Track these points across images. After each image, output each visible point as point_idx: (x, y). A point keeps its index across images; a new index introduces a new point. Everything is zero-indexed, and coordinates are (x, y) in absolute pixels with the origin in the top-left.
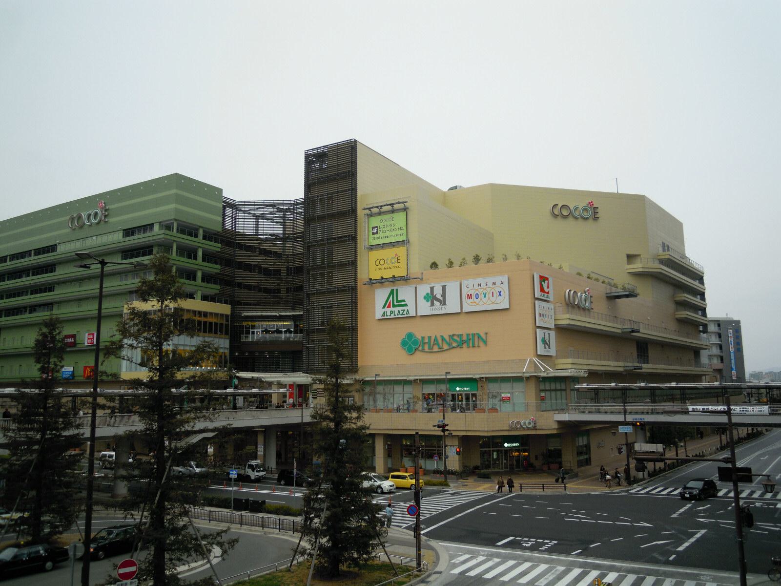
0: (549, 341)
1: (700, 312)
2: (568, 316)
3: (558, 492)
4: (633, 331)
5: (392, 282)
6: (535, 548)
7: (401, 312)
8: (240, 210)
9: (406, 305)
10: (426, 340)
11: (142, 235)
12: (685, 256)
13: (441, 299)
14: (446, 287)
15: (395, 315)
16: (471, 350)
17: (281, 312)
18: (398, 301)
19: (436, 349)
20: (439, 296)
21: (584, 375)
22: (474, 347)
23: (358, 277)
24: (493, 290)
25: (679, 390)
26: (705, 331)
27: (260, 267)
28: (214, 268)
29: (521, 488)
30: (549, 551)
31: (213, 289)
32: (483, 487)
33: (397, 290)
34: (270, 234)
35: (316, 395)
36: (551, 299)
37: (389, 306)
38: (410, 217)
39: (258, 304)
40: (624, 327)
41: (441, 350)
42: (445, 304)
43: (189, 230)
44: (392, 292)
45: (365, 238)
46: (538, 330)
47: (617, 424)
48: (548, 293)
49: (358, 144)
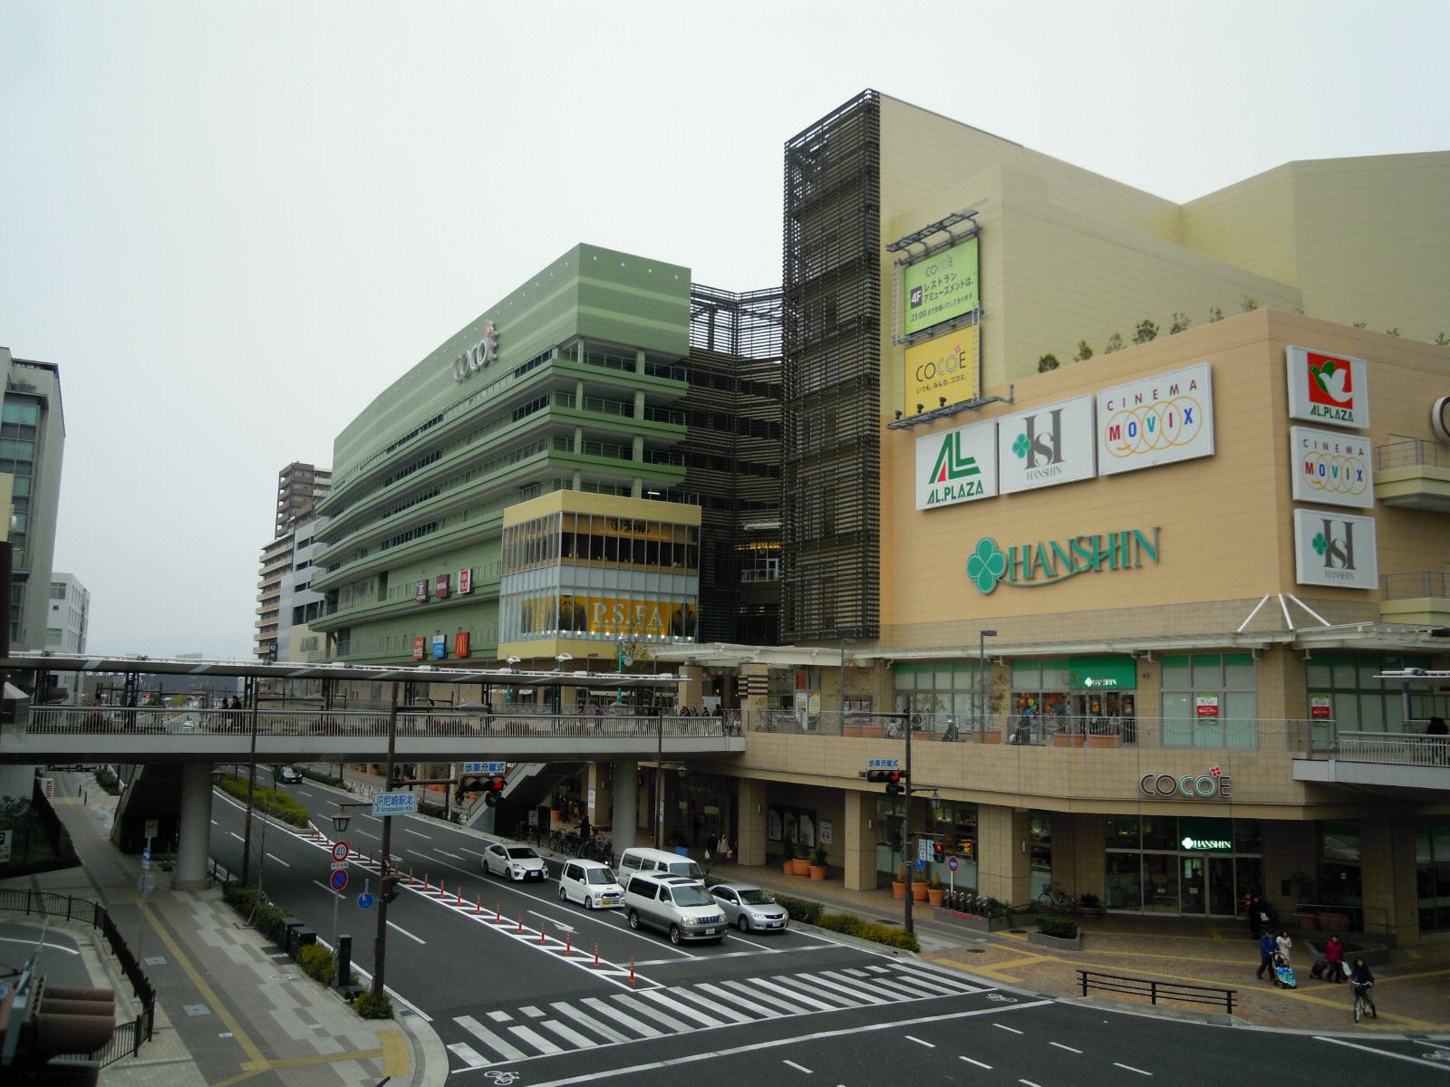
2: (1418, 470)
3: (1199, 1015)
7: (966, 489)
8: (745, 312)
9: (976, 470)
13: (1050, 445)
14: (1062, 413)
15: (953, 498)
16: (1122, 575)
18: (960, 463)
19: (1041, 578)
20: (1046, 441)
22: (1128, 568)
23: (881, 413)
24: (1171, 409)
28: (672, 432)
29: (1085, 987)
31: (673, 474)
33: (958, 434)
35: (746, 685)
36: (1361, 417)
37: (942, 478)
38: (986, 252)
41: (1053, 579)
42: (1058, 459)
45: (897, 319)
46: (1298, 512)
48: (1349, 404)
49: (882, 99)
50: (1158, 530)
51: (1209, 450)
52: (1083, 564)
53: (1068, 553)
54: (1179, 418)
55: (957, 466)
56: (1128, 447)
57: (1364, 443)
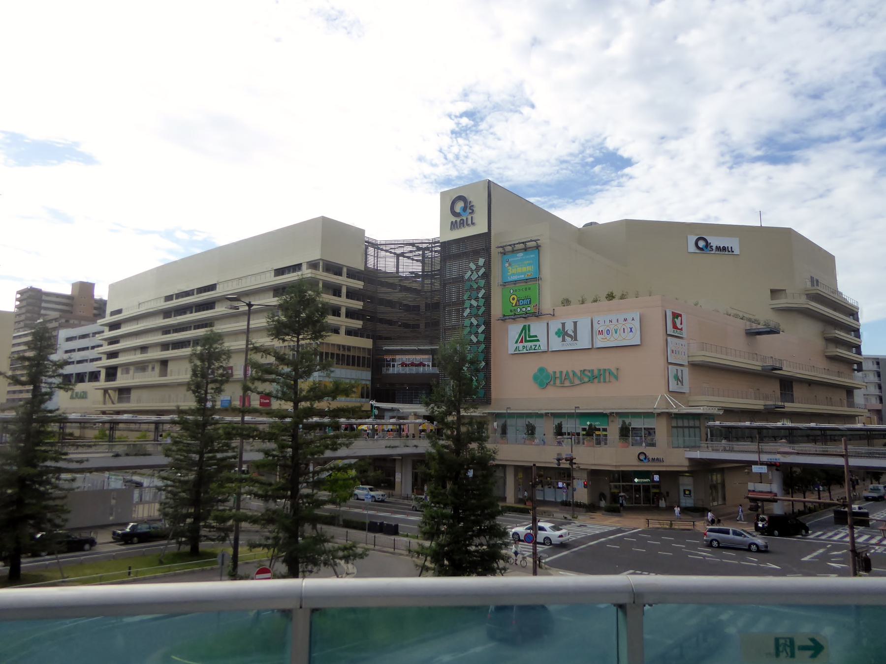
0: (682, 378)
1: (854, 349)
5: (524, 318)
7: (533, 347)
8: (382, 250)
9: (538, 340)
10: (558, 375)
12: (838, 291)
13: (573, 334)
17: (420, 346)
18: (530, 337)
21: (719, 412)
22: (605, 382)
24: (624, 327)
26: (860, 369)
27: (401, 304)
32: (610, 521)
33: (529, 326)
34: (410, 272)
36: (684, 336)
37: (522, 342)
39: (401, 339)
41: (572, 384)
42: (576, 339)
43: (333, 268)
44: (524, 328)
47: (750, 463)
48: (681, 329)
50: (618, 369)
51: (639, 343)
53: (580, 375)
54: (627, 330)
55: (529, 338)
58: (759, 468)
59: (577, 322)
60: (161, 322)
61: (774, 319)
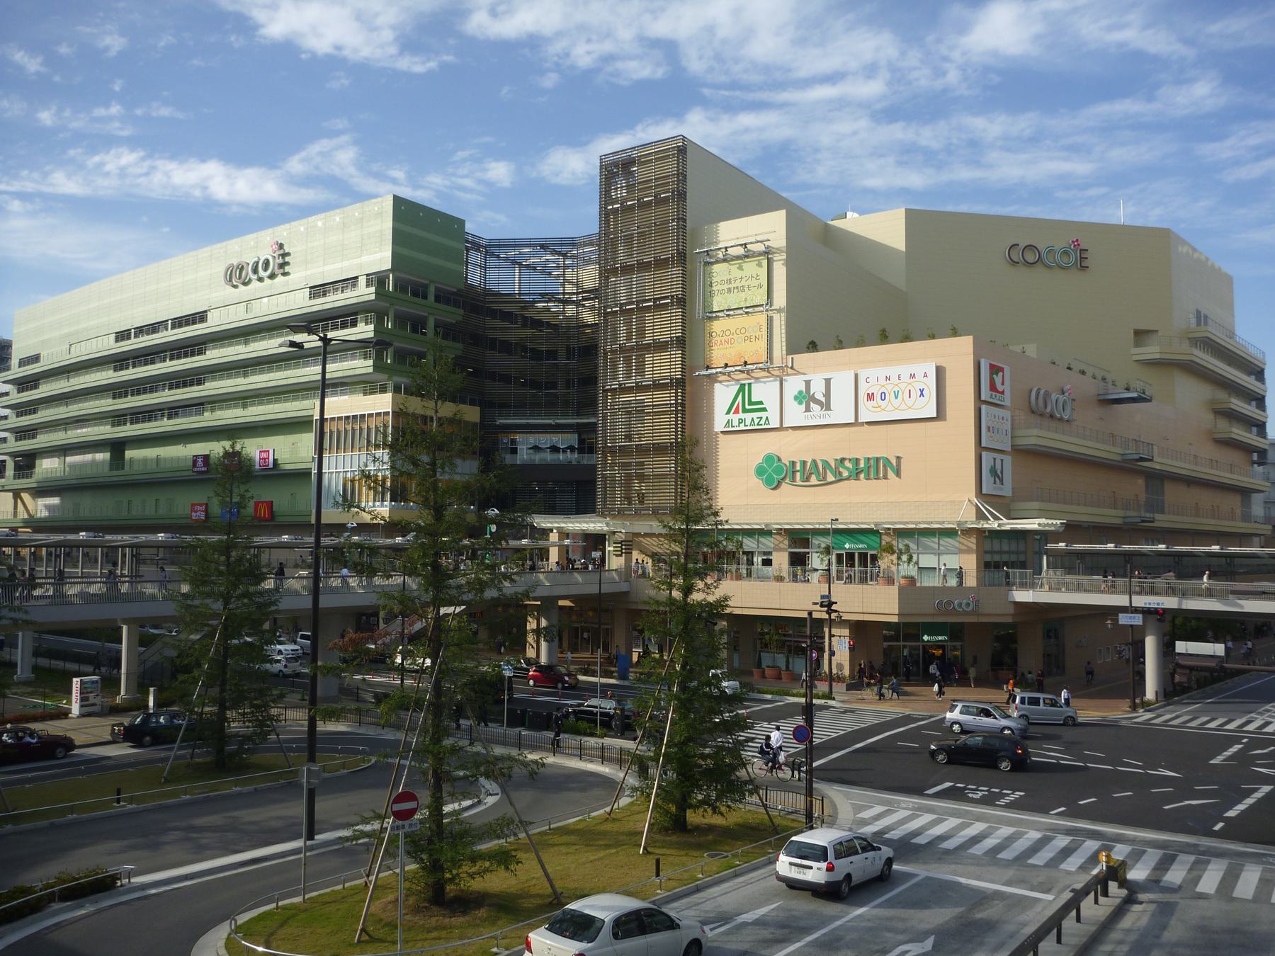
0: (1002, 473)
2: (1035, 432)
4: (1142, 459)
6: (988, 801)
9: (764, 410)
11: (339, 296)
13: (823, 400)
15: (745, 426)
18: (751, 403)
19: (814, 480)
20: (820, 396)
22: (877, 478)
24: (910, 387)
25: (1224, 559)
30: (1011, 806)
36: (1007, 402)
37: (737, 412)
40: (1127, 452)
42: (828, 408)
46: (984, 454)
48: (1003, 393)
52: (846, 474)
54: (917, 393)
56: (880, 407)
57: (1006, 414)
58: (1130, 618)
59: (830, 379)
60: (107, 376)
61: (1141, 380)
